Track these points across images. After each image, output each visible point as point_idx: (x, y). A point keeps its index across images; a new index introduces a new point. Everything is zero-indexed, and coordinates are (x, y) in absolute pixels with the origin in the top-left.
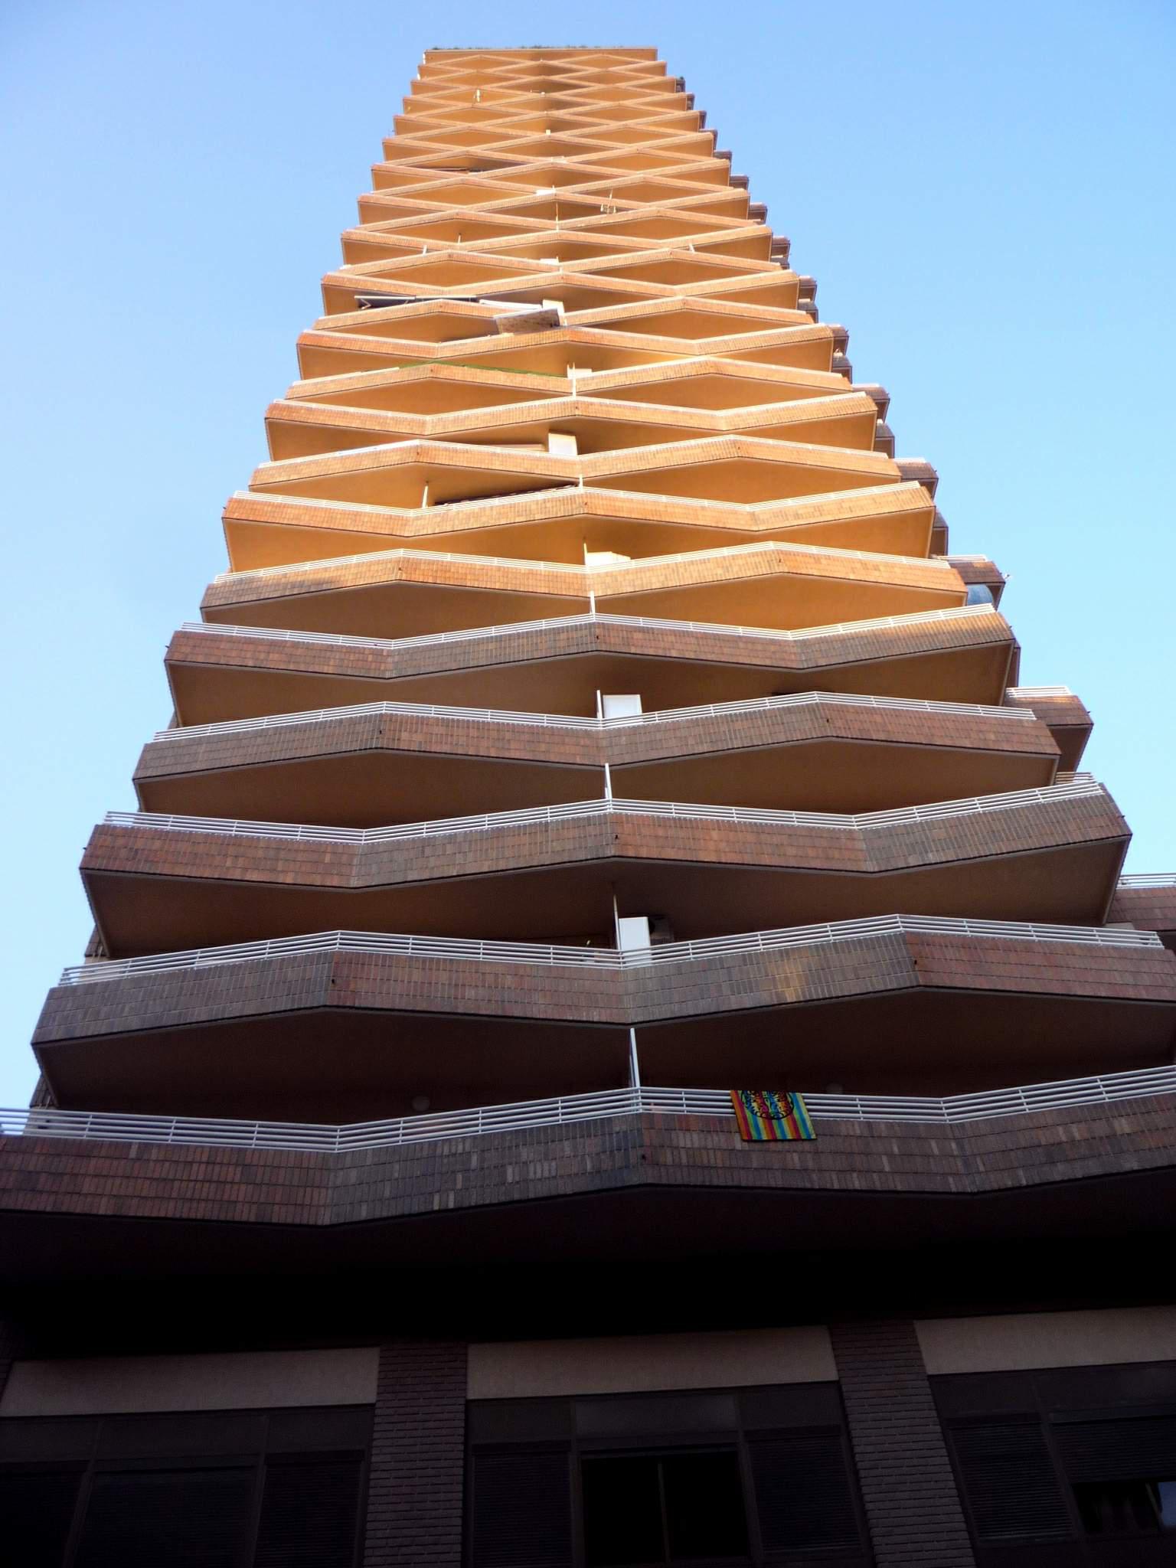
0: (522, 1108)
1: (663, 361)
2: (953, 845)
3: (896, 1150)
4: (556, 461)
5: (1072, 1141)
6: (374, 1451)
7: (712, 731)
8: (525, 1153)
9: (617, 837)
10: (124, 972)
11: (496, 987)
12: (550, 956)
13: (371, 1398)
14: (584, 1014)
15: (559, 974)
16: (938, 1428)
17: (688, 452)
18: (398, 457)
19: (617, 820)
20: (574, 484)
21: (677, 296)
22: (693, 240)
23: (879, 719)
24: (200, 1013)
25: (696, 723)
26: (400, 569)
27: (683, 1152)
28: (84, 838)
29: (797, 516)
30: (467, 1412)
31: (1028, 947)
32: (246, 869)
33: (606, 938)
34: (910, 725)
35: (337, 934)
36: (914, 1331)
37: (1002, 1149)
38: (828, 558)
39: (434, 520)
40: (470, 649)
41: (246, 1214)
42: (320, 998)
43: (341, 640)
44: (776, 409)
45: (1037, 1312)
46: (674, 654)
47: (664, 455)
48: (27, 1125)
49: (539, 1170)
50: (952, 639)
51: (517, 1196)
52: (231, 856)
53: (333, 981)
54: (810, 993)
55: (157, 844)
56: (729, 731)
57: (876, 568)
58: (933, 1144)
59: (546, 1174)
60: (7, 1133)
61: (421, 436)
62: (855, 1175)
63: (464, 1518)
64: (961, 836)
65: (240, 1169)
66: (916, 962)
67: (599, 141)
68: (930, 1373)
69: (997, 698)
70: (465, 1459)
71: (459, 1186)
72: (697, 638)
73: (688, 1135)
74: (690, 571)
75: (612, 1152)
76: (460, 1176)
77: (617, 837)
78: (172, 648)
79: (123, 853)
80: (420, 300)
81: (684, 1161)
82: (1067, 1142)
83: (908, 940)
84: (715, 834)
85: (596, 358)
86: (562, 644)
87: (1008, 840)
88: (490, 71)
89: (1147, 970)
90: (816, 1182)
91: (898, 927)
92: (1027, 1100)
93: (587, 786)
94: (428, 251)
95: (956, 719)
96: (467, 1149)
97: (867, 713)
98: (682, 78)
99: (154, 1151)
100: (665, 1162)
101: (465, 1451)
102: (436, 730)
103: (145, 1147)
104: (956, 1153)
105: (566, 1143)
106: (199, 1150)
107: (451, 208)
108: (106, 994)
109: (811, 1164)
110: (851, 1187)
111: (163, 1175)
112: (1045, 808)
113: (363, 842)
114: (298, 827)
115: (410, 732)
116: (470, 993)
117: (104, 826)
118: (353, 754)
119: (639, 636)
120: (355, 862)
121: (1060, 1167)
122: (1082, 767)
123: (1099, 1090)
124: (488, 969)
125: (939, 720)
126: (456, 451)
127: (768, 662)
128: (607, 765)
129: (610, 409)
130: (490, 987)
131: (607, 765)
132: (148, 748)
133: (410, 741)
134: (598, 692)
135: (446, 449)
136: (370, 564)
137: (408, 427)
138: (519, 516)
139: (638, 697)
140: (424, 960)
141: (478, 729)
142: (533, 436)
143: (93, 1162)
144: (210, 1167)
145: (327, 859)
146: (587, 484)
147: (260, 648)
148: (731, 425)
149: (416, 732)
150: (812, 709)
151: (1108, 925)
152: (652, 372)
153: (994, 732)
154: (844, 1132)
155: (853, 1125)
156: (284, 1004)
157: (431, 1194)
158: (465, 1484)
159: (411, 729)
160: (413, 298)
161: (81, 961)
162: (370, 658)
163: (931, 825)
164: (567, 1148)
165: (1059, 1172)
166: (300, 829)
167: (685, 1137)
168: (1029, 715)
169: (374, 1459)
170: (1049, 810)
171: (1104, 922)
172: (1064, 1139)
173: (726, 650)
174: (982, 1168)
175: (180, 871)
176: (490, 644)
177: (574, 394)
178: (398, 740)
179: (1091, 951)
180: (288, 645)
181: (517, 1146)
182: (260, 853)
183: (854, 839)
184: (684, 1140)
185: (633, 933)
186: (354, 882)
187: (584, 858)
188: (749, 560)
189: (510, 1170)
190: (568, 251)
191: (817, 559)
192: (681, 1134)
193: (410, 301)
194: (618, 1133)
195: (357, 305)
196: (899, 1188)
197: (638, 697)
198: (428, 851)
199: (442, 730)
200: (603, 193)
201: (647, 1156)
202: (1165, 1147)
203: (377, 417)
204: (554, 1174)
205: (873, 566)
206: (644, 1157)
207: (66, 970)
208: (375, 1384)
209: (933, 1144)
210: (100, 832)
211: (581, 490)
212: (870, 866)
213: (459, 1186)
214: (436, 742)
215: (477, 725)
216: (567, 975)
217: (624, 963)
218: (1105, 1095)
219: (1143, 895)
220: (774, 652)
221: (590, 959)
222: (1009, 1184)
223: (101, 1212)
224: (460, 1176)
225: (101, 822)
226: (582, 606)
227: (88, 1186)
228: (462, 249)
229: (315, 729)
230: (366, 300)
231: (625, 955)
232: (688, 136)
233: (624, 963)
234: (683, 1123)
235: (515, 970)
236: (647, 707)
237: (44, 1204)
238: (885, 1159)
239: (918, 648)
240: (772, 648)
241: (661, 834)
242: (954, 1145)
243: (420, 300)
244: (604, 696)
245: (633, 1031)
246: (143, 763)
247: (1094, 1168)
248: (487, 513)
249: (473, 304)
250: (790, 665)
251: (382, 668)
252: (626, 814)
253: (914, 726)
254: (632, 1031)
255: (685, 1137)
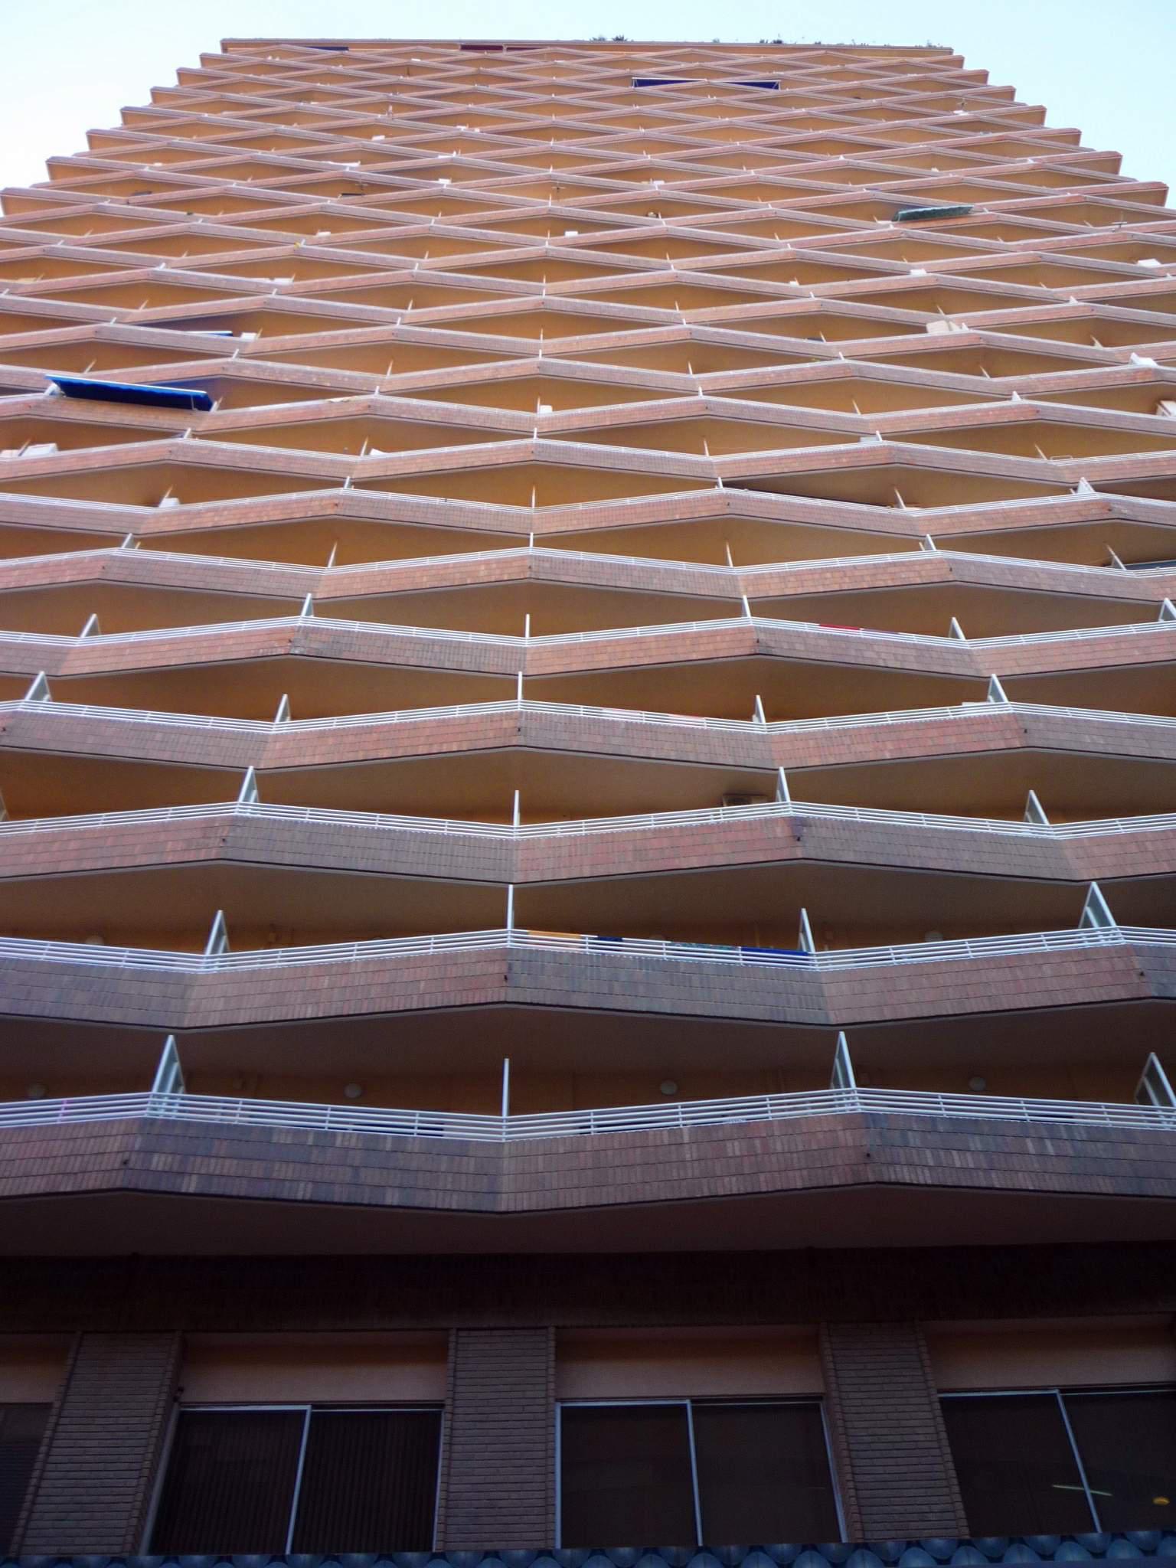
0: (1150, 1111)
1: (105, 452)
40: (423, 655)
44: (573, 448)
67: (497, 126)
91: (662, 953)
107: (543, 144)
114: (375, 816)
123: (939, 1106)
232: (440, 157)
245: (842, 1035)
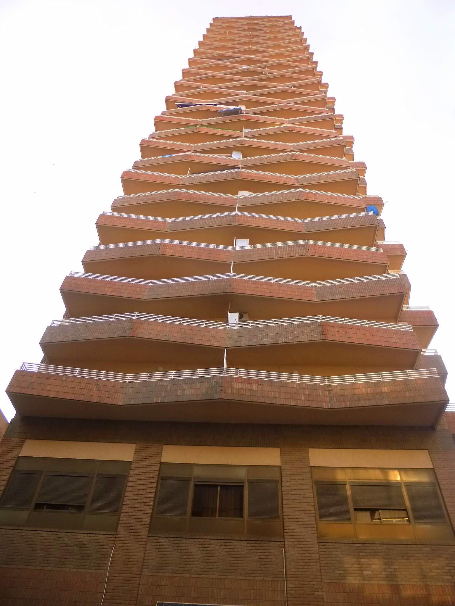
2: (345, 293)
3: (307, 393)
4: (233, 160)
5: (367, 393)
6: (130, 475)
7: (269, 252)
8: (185, 386)
9: (231, 286)
10: (70, 322)
11: (184, 333)
12: (204, 324)
13: (130, 459)
14: (212, 343)
15: (205, 330)
16: (311, 483)
17: (277, 158)
18: (181, 158)
19: (232, 280)
20: (238, 168)
21: (284, 103)
22: (293, 84)
23: (326, 250)
24: (90, 336)
25: (265, 249)
26: (175, 195)
27: (235, 390)
28: (62, 279)
29: (312, 180)
30: (160, 466)
31: (364, 328)
32: (111, 292)
33: (225, 318)
34: (337, 252)
35: (136, 314)
36: (308, 452)
37: (343, 395)
38: (319, 194)
39: (190, 179)
41: (96, 400)
42: (127, 333)
43: (153, 218)
45: (367, 449)
46: (261, 226)
47: (270, 158)
48: (39, 369)
49: (189, 392)
50: (357, 224)
51: (180, 400)
52: (107, 287)
53: (132, 328)
54: (285, 340)
55: (85, 282)
56: (275, 252)
57: (336, 198)
58: (320, 392)
59: (190, 393)
60: (28, 370)
61: (190, 151)
62: (291, 400)
63: (155, 498)
64: (348, 291)
65: (96, 386)
66: (323, 332)
68: (311, 466)
69: (373, 244)
70: (158, 481)
71: (163, 395)
72: (270, 221)
73: (237, 384)
74: (272, 198)
75: (212, 388)
76: (163, 393)
77: (231, 286)
78: (99, 220)
79: (74, 285)
80: (197, 105)
81: (235, 392)
82: (365, 394)
83: (322, 324)
84: (264, 286)
85: (253, 124)
86: (224, 221)
87: (364, 292)
88: (276, 23)
89: (405, 338)
90: (278, 401)
92: (355, 379)
93: (224, 267)
94: (202, 88)
95: (354, 250)
96: (167, 384)
97: (323, 248)
98: (301, 26)
99: (70, 379)
100: (345, 394)
101: (158, 478)
102: (178, 248)
103: (68, 377)
104: (328, 395)
105: (198, 384)
106: (84, 379)
108: (63, 329)
109: (277, 396)
110: (289, 404)
111: (72, 386)
112: (392, 280)
113: (151, 284)
115: (170, 249)
116: (175, 335)
117: (69, 276)
118: (150, 256)
119: (250, 219)
120: (147, 291)
121: (362, 402)
122: (402, 269)
124: (182, 327)
125: (348, 251)
126: (200, 156)
127: (293, 229)
128: (232, 262)
129: (254, 143)
130: (182, 333)
131: (232, 262)
132: (88, 252)
133: (169, 252)
134: (235, 238)
135: (197, 156)
136: (166, 193)
137: (186, 148)
138: (217, 178)
139: (248, 240)
140: (162, 323)
141: (192, 249)
142: (228, 150)
143: (51, 381)
144: (87, 384)
145: (138, 289)
146: (241, 168)
147: (127, 220)
148: (295, 149)
149: (171, 249)
150: (304, 246)
151: (399, 323)
152: (270, 130)
153: (366, 256)
154: (290, 386)
155: (294, 384)
156: (116, 335)
157: (154, 397)
158: (156, 488)
159: (170, 248)
160: (195, 104)
161: (62, 318)
162: (162, 224)
163: (338, 286)
164: (198, 386)
165: (362, 403)
166: (131, 280)
167: (236, 384)
168: (381, 250)
169: (129, 478)
170: (380, 283)
171: (398, 321)
172: (364, 392)
173: (279, 225)
174: (335, 401)
175: (91, 291)
176: (201, 221)
177: (243, 137)
178: (165, 251)
179: (387, 331)
180: (136, 220)
181: (183, 384)
182: (117, 287)
183: (312, 290)
184: (237, 385)
185: (233, 317)
186: (145, 297)
187: (219, 292)
188: (292, 195)
189: (179, 391)
190: (249, 87)
191: (315, 195)
192: (235, 383)
193: (194, 105)
194: (215, 382)
195: (177, 106)
196: (306, 405)
197: (248, 240)
198: (170, 288)
199: (180, 249)
200: (264, 67)
201: (223, 390)
202: (398, 398)
203: (177, 144)
204: (192, 394)
205: (335, 197)
206: (222, 390)
207: (53, 321)
208: (133, 455)
209: (320, 392)
210: (67, 278)
211: (240, 170)
212: (316, 299)
213: (163, 395)
214: (178, 253)
215: (192, 247)
216: (208, 331)
217: (228, 327)
218: (381, 379)
219: (414, 313)
220: (296, 226)
221: (218, 326)
222: (344, 406)
223: (52, 396)
224: (163, 393)
225: (68, 275)
226: (233, 209)
227: (49, 388)
228: (213, 87)
229: (140, 247)
230: (179, 105)
231: (229, 325)
233: (228, 327)
234: (237, 380)
235: (192, 328)
236: (250, 243)
237: (35, 392)
238: (303, 396)
239: (341, 226)
240: (296, 225)
241: (246, 286)
242: (327, 393)
243: (197, 105)
244: (237, 239)
246: (85, 256)
247: (373, 403)
248: (208, 177)
249: (215, 106)
250: (300, 230)
251: (165, 228)
252: (235, 278)
253: (338, 252)
254: (226, 349)
255: (236, 384)
